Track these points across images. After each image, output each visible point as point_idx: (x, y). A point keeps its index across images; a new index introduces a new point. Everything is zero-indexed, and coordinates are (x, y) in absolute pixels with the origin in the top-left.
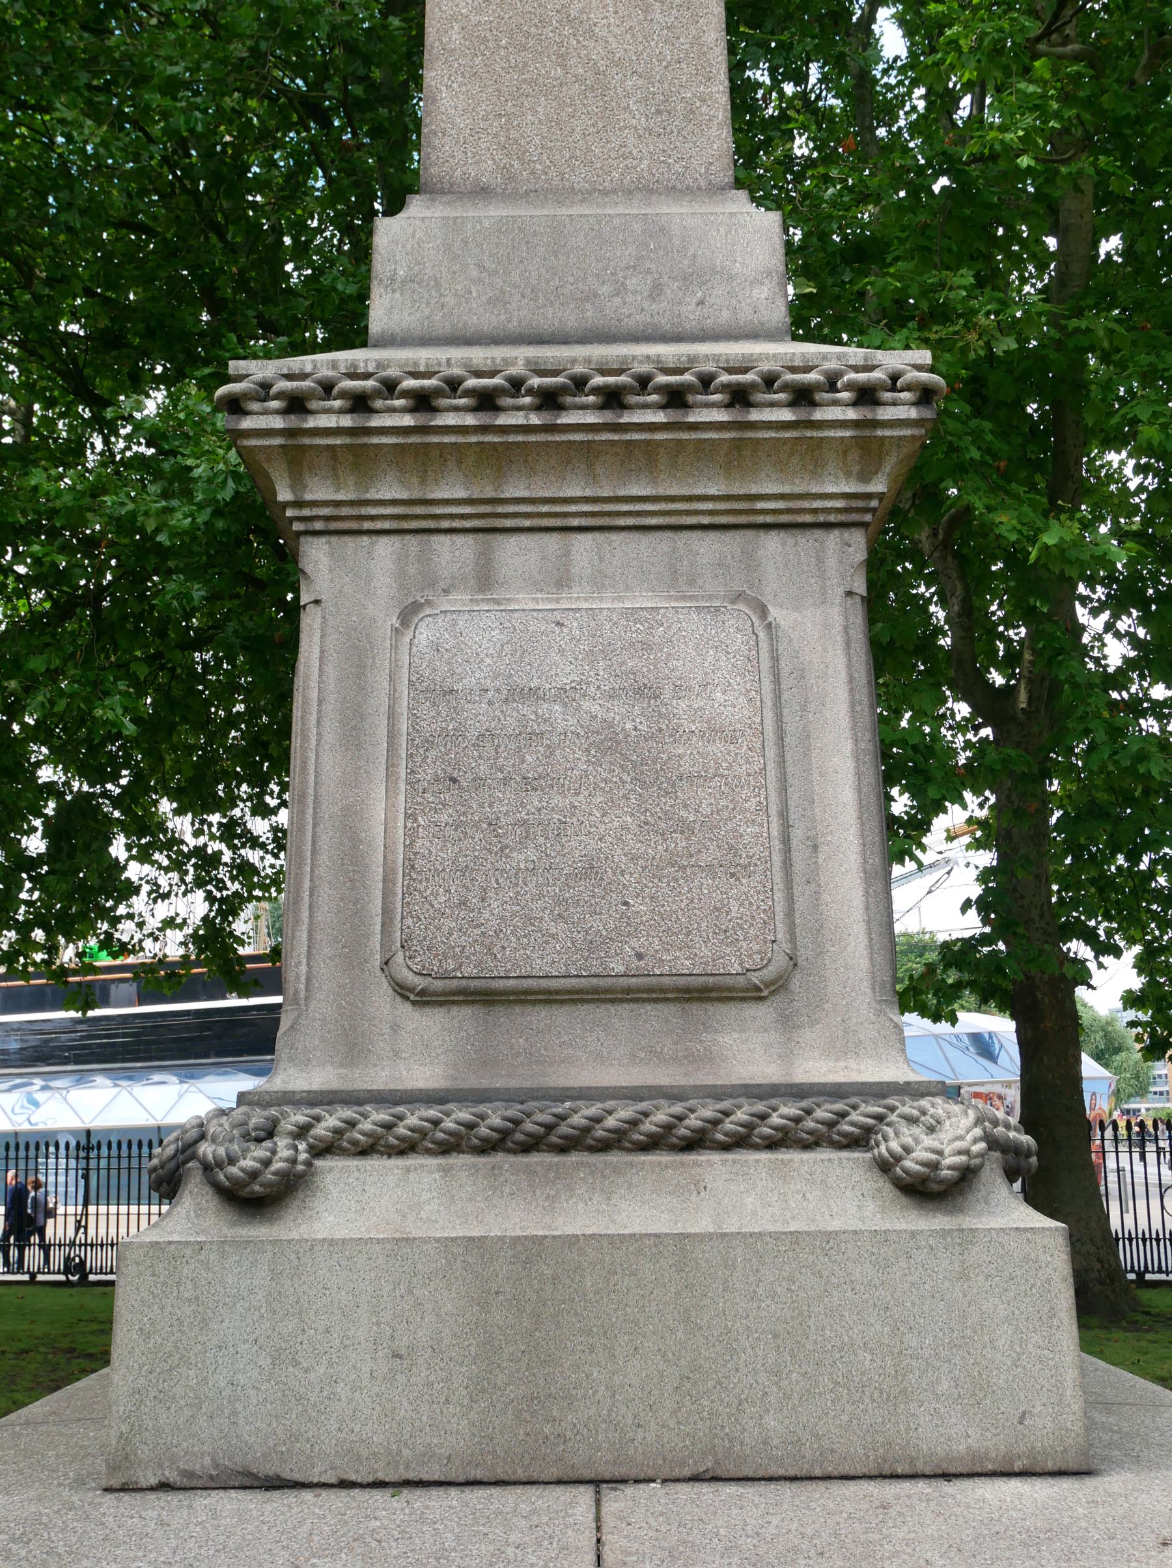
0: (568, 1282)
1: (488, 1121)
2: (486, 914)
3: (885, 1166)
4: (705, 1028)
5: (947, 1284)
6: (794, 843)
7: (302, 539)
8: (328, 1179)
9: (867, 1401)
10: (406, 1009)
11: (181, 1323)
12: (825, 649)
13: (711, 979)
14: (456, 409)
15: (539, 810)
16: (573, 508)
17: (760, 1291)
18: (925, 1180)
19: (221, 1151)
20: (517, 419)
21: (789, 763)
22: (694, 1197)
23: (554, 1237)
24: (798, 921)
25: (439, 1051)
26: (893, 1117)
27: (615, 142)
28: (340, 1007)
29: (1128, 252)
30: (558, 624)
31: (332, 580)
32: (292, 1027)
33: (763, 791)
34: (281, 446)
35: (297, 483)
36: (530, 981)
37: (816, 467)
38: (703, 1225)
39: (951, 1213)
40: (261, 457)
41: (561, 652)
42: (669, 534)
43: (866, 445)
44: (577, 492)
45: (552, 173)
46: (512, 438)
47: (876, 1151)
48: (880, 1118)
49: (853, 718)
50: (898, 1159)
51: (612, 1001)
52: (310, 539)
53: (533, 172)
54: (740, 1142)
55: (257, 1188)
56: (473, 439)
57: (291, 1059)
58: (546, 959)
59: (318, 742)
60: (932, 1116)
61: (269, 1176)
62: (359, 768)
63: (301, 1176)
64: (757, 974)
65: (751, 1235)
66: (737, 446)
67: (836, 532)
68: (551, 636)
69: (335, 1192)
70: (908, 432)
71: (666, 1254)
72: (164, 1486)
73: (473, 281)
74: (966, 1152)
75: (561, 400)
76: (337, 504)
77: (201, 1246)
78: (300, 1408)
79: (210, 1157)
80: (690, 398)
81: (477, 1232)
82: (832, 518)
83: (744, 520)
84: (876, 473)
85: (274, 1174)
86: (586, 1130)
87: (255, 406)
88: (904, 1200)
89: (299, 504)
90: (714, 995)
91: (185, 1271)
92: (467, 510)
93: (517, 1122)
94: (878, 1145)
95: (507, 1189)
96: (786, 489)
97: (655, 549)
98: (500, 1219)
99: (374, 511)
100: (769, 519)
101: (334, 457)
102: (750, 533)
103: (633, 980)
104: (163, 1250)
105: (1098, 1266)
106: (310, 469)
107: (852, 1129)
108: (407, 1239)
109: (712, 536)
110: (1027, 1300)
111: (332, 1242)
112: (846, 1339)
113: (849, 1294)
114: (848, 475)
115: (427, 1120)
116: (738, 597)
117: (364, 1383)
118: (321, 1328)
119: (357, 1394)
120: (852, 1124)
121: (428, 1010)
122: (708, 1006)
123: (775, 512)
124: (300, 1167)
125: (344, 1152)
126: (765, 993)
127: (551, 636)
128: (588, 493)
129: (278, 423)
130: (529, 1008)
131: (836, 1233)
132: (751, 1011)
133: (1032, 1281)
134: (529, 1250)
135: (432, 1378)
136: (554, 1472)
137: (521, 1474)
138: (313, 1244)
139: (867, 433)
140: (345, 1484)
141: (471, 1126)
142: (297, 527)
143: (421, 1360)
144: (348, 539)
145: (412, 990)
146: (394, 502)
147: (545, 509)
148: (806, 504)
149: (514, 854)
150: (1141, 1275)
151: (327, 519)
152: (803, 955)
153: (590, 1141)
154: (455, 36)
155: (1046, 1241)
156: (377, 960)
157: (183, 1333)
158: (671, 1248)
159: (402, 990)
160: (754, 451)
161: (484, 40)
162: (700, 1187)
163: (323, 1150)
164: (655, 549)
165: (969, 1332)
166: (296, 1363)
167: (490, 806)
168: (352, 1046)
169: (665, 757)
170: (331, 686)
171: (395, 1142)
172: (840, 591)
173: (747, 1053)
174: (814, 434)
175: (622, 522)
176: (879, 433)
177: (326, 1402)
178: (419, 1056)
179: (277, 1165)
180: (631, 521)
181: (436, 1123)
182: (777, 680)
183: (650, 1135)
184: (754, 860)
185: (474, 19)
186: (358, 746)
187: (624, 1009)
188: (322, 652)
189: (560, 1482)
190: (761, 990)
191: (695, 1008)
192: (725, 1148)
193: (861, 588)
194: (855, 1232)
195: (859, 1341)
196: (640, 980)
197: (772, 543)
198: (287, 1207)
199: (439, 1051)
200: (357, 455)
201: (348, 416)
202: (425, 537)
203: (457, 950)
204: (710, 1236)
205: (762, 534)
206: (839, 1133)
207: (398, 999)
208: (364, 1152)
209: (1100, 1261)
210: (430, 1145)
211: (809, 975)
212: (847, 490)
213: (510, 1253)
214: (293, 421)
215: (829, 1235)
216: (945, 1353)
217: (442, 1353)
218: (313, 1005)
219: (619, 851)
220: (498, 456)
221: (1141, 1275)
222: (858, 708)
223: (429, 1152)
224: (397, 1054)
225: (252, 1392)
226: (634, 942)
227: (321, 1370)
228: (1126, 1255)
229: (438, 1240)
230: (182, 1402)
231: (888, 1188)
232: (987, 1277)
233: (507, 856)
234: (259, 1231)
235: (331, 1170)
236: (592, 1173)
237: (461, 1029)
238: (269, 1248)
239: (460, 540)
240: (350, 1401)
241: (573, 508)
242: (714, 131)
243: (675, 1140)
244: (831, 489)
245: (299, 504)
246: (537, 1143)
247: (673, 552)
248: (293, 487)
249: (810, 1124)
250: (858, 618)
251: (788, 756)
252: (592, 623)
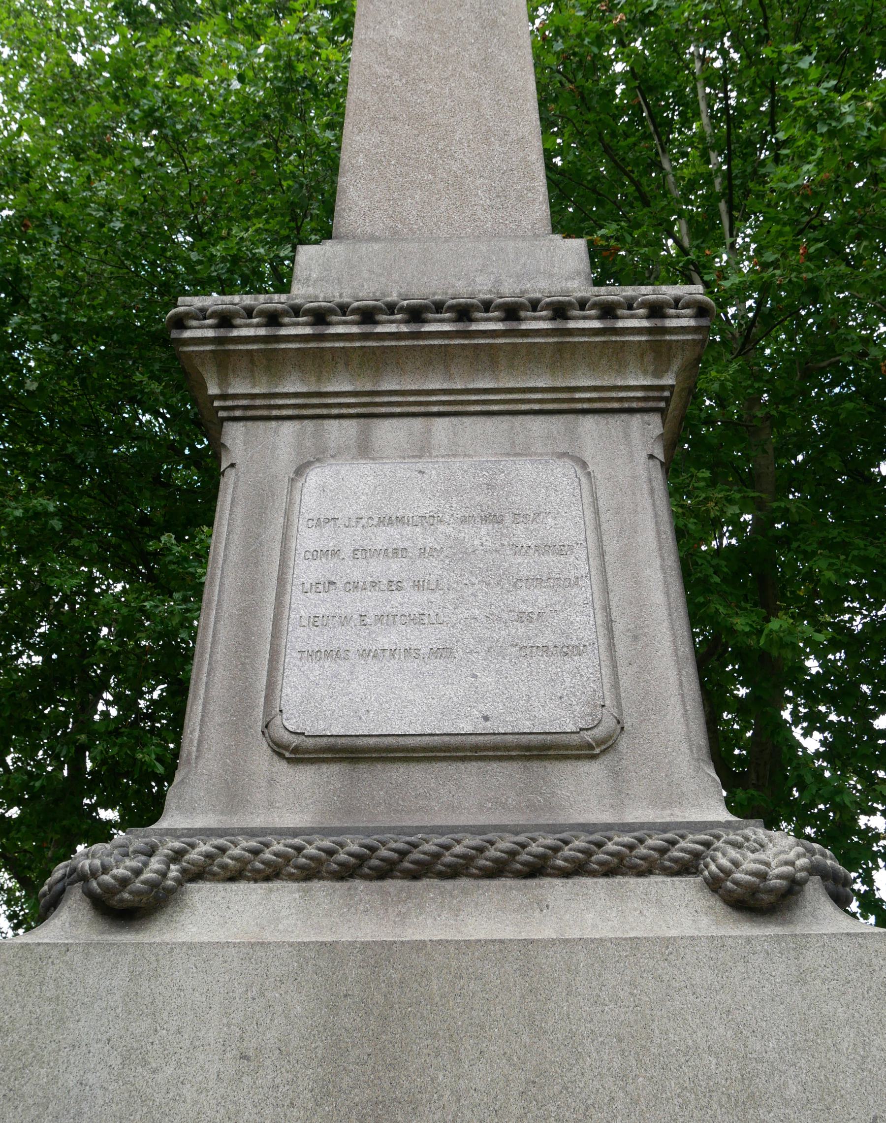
0: (415, 985)
1: (347, 848)
2: (354, 685)
3: (715, 885)
4: (545, 783)
5: (786, 988)
6: (617, 633)
7: (225, 424)
8: (196, 897)
9: (715, 1106)
10: (282, 766)
11: (39, 1023)
12: (634, 494)
13: (549, 737)
14: (345, 323)
15: (401, 605)
16: (434, 398)
17: (603, 995)
18: (753, 891)
19: (97, 862)
20: (392, 328)
21: (610, 574)
22: (537, 913)
23: (402, 942)
24: (623, 695)
25: (309, 802)
26: (718, 844)
27: (468, 212)
28: (225, 763)
30: (420, 472)
31: (245, 450)
32: (182, 781)
33: (589, 590)
34: (212, 351)
35: (223, 380)
36: (390, 739)
37: (621, 368)
38: (548, 932)
39: (784, 923)
40: (197, 361)
41: (422, 491)
43: (658, 348)
44: (438, 386)
45: (425, 229)
46: (387, 343)
47: (706, 873)
48: (707, 845)
49: (659, 541)
50: (727, 873)
51: (463, 759)
52: (231, 423)
53: (411, 230)
55: (126, 896)
56: (357, 344)
57: (178, 808)
59: (224, 561)
60: (755, 841)
61: (138, 885)
62: (256, 580)
63: (171, 891)
64: (589, 732)
65: (592, 940)
66: (560, 348)
67: (638, 415)
68: (415, 480)
69: (201, 908)
70: (690, 337)
71: (511, 959)
73: (365, 280)
74: (792, 864)
75: (424, 316)
77: (67, 947)
78: (145, 1109)
79: (87, 868)
80: (523, 314)
81: (329, 938)
82: (634, 405)
83: (567, 406)
84: (667, 371)
85: (143, 883)
86: (437, 856)
87: (194, 323)
88: (736, 915)
89: (224, 397)
90: (551, 752)
91: (50, 972)
93: (373, 849)
94: (707, 866)
95: (361, 907)
96: (598, 383)
97: (497, 427)
98: (352, 931)
99: (280, 402)
100: (586, 406)
101: (252, 361)
102: (571, 417)
103: (481, 738)
104: (31, 951)
106: (234, 371)
107: (681, 854)
108: (262, 944)
109: (541, 419)
110: (865, 1003)
111: (191, 946)
112: (690, 1043)
113: (691, 998)
114: (645, 373)
115: (291, 846)
116: (564, 455)
117: (211, 1084)
118: (173, 1029)
119: (203, 1096)
120: (682, 850)
121: (301, 767)
122: (546, 763)
123: (589, 400)
124: (170, 883)
125: (214, 877)
126: (597, 751)
127: (415, 480)
128: (445, 386)
129: (210, 333)
130: (389, 766)
131: (675, 938)
132: (585, 767)
133: (867, 984)
134: (378, 954)
135: (278, 1081)
138: (172, 947)
139: (658, 338)
141: (330, 853)
142: (221, 414)
143: (268, 1062)
144: (261, 424)
145: (286, 748)
146: (296, 395)
148: (614, 394)
149: (380, 638)
151: (245, 408)
152: (628, 723)
153: (440, 867)
154: (361, 159)
155: (877, 946)
156: (260, 724)
157: (40, 1031)
158: (516, 954)
159: (279, 749)
160: (573, 354)
161: (381, 161)
162: (542, 905)
163: (197, 874)
164: (497, 427)
165: (811, 1036)
166: (145, 1063)
167: (360, 602)
169: (507, 565)
170: (239, 522)
171: (261, 866)
172: (644, 454)
173: (584, 799)
174: (618, 339)
175: (472, 408)
176: (668, 338)
177: (172, 1103)
178: (292, 805)
179: (147, 875)
180: (478, 408)
181: (299, 849)
182: (597, 512)
183: (496, 861)
184: (583, 642)
185: (373, 151)
186: (256, 564)
187: (473, 767)
188: (233, 498)
190: (593, 748)
191: (536, 766)
192: (564, 874)
193: (660, 454)
194: (692, 938)
195: (703, 1045)
196: (487, 738)
197: (588, 423)
198: (155, 920)
199: (309, 802)
200: (269, 358)
201: (264, 329)
202: (320, 421)
203: (328, 713)
204: (553, 942)
205: (580, 417)
206: (671, 860)
207: (276, 758)
208: (234, 877)
210: (293, 870)
211: (635, 738)
212: (645, 383)
213: (360, 957)
214: (222, 332)
215: (668, 941)
216: (789, 1057)
217: (289, 1054)
218: (201, 763)
219: (468, 635)
220: (378, 358)
222: (664, 536)
223: (292, 878)
224: (271, 804)
225: (99, 1092)
226: (481, 707)
227: (169, 1070)
229: (291, 945)
230: (30, 1101)
231: (719, 905)
232: (824, 981)
233: (374, 640)
234: (127, 937)
235: (199, 891)
236: (441, 893)
237: (329, 783)
238: (131, 950)
239: (346, 423)
240: (195, 1103)
242: (536, 207)
243: (518, 866)
244: (632, 382)
246: (392, 870)
247: (512, 429)
248: (220, 386)
249: (642, 850)
250: (658, 475)
251: (608, 570)
252: (448, 471)
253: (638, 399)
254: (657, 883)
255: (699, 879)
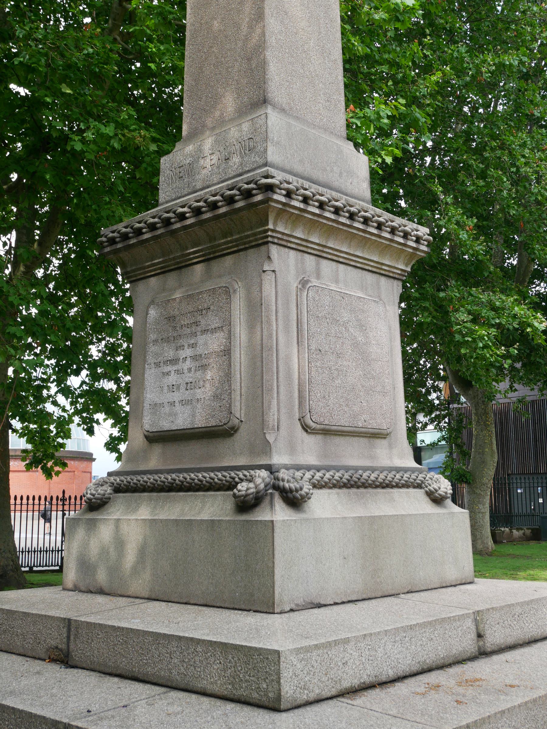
16: (342, 255)
29: (144, 103)
35: (275, 224)
42: (360, 271)
54: (397, 486)
56: (330, 223)
58: (342, 420)
72: (292, 610)
76: (283, 234)
89: (273, 231)
92: (316, 247)
105: (12, 563)
106: (294, 221)
109: (370, 274)
128: (347, 251)
136: (380, 594)
137: (373, 596)
140: (336, 604)
147: (336, 253)
150: (31, 568)
151: (279, 239)
159: (306, 428)
168: (292, 449)
189: (382, 597)
197: (383, 280)
200: (297, 218)
209: (13, 561)
220: (331, 231)
221: (31, 568)
224: (303, 451)
228: (23, 559)
241: (342, 255)
245: (273, 231)
253: (398, 274)
254: (411, 490)
255: (422, 490)
